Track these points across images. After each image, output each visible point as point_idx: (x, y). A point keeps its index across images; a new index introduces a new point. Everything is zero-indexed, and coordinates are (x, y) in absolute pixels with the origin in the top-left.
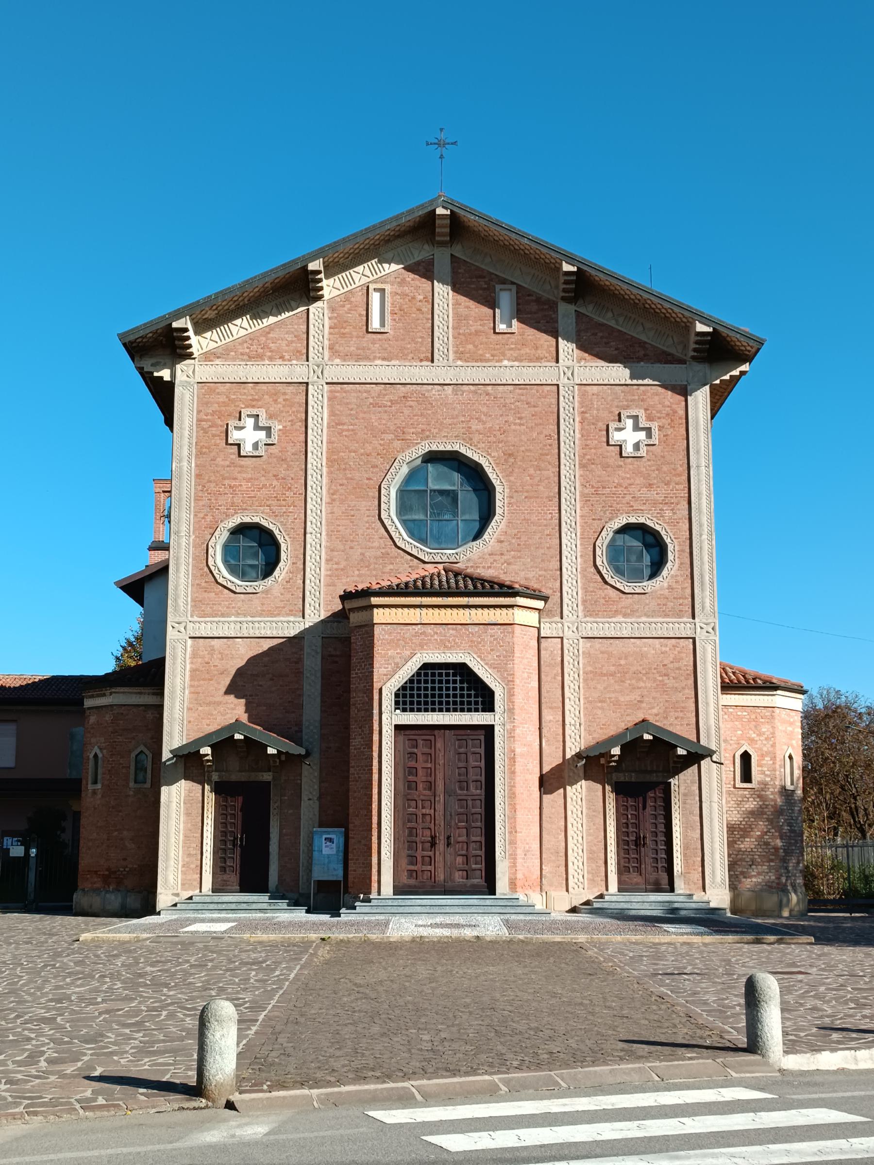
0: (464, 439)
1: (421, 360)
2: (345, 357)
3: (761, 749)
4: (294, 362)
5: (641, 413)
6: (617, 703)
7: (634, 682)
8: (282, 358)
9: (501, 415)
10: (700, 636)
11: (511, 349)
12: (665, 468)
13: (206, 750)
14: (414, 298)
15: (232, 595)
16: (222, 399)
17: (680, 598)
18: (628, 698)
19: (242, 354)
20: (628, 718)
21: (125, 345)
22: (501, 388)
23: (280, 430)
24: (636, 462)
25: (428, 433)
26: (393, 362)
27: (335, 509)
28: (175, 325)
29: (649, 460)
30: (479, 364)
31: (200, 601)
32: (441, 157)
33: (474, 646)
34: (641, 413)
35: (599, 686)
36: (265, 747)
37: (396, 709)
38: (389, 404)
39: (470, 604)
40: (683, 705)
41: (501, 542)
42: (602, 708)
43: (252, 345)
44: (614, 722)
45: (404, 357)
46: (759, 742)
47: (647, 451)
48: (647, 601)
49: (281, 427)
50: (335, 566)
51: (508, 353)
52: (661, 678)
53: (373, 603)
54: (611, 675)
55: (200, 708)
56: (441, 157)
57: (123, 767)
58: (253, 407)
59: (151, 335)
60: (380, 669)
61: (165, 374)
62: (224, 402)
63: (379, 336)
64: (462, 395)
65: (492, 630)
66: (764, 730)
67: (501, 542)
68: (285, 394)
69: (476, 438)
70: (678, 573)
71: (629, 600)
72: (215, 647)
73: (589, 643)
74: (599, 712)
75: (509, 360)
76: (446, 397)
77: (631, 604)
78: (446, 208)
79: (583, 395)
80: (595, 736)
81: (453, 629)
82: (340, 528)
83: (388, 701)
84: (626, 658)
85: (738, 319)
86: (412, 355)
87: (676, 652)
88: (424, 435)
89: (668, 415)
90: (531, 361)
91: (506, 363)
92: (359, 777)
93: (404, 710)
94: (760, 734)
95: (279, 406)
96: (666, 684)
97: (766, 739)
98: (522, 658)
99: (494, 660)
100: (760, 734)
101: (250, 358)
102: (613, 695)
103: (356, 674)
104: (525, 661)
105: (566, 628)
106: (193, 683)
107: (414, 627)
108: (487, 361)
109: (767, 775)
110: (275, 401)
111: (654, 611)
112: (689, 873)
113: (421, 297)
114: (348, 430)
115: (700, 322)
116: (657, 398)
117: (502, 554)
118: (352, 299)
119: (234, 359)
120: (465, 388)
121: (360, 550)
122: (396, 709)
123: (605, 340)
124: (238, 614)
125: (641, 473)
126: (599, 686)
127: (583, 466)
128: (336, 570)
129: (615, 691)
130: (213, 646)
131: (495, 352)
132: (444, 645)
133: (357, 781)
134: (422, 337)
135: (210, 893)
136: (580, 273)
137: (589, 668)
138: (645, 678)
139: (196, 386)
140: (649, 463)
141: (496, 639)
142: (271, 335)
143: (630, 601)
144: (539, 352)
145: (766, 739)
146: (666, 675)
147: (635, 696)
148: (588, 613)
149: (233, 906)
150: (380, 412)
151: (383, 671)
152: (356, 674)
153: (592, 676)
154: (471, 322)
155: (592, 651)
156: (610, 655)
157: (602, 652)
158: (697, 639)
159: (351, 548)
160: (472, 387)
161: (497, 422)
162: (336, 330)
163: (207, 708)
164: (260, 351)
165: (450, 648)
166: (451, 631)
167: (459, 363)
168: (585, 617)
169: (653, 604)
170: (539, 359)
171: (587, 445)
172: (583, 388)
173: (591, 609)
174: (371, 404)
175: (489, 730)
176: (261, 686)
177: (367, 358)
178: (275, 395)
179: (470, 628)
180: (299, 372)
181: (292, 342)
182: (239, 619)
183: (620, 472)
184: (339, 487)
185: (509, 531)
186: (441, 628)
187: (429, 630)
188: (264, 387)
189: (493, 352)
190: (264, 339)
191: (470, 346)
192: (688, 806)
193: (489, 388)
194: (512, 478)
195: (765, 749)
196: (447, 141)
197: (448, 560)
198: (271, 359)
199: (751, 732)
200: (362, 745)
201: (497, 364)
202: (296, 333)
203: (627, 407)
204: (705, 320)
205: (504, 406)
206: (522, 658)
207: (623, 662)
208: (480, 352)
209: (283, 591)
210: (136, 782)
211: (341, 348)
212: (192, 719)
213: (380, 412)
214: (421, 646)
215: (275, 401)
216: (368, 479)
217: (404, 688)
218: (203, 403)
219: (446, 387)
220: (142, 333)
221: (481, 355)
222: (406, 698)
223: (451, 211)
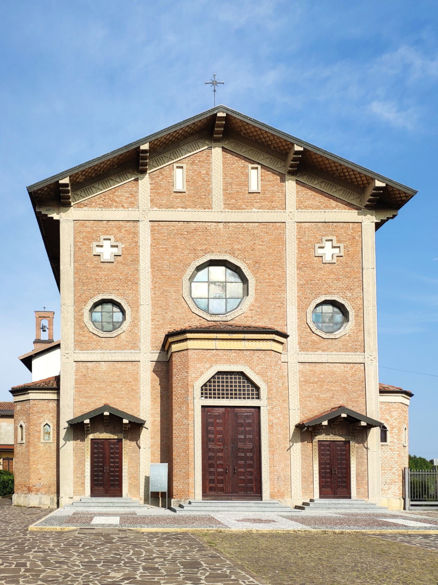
0: (230, 254)
1: (204, 209)
2: (160, 206)
3: (392, 425)
4: (131, 209)
5: (334, 238)
6: (318, 398)
7: (328, 387)
8: (123, 206)
9: (251, 240)
10: (367, 361)
11: (257, 202)
12: (348, 270)
13: (125, 421)
14: (200, 172)
15: (98, 338)
16: (89, 230)
17: (355, 342)
18: (325, 396)
19: (99, 204)
20: (325, 406)
21: (30, 194)
22: (251, 224)
23: (123, 248)
24: (332, 266)
25: (209, 250)
26: (188, 209)
27: (156, 292)
28: (61, 182)
29: (338, 265)
30: (239, 211)
31: (80, 342)
32: (215, 91)
33: (248, 363)
34: (334, 238)
35: (308, 389)
36: (122, 419)
37: (201, 397)
38: (186, 233)
39: (246, 338)
40: (357, 400)
41: (252, 310)
42: (309, 401)
43: (105, 199)
44: (318, 407)
45: (195, 206)
46: (391, 421)
47: (337, 260)
48: (336, 343)
49: (123, 246)
50: (157, 323)
51: (256, 205)
52: (344, 385)
53: (188, 337)
54: (315, 383)
55: (81, 400)
56: (215, 91)
57: (37, 432)
58: (107, 234)
59: (46, 189)
60: (192, 374)
61: (55, 216)
62: (89, 232)
63: (180, 194)
64: (229, 228)
65: (257, 354)
66: (394, 415)
67: (252, 310)
68: (126, 227)
69: (237, 253)
70: (354, 328)
71: (326, 342)
72: (89, 367)
73: (302, 366)
74: (308, 403)
75: (256, 208)
76: (220, 230)
77: (327, 345)
78: (224, 112)
79: (299, 228)
80: (306, 416)
81: (235, 353)
82: (159, 302)
83: (198, 392)
84: (324, 374)
85: (401, 178)
86: (198, 205)
87: (353, 371)
88: (206, 252)
89: (350, 239)
90: (269, 209)
91: (254, 210)
92: (180, 435)
93: (206, 397)
94: (392, 417)
95: (122, 234)
96: (347, 388)
97: (395, 419)
98: (275, 370)
99: (259, 370)
100: (392, 417)
101: (105, 207)
102: (317, 394)
103: (176, 378)
104: (276, 371)
105: (289, 357)
106: (77, 386)
107: (212, 351)
108: (244, 209)
109: (394, 438)
110: (120, 231)
111: (340, 349)
112: (359, 489)
113: (204, 172)
114: (162, 248)
115: (378, 180)
116: (343, 230)
117: (252, 317)
118: (164, 173)
119: (95, 207)
120: (230, 224)
121: (171, 314)
122: (201, 397)
123: (313, 197)
124: (101, 349)
125: (334, 272)
126: (308, 389)
127: (299, 268)
128: (158, 325)
129: (318, 392)
130: (88, 366)
131: (248, 204)
132: (228, 361)
133: (178, 437)
134: (205, 195)
135: (90, 497)
136: (305, 152)
137: (302, 379)
138: (335, 385)
139: (72, 222)
140: (338, 267)
141: (261, 358)
142: (116, 193)
143: (326, 343)
144: (274, 204)
145: (395, 419)
146: (347, 383)
147: (329, 394)
148: (302, 349)
149: (105, 504)
150: (181, 238)
151: (193, 375)
152: (176, 378)
153: (305, 382)
154: (234, 187)
155: (304, 370)
156: (315, 372)
157: (311, 371)
158: (366, 364)
159: (166, 313)
160: (234, 224)
161: (249, 243)
162: (154, 191)
163: (85, 400)
164: (110, 202)
165: (232, 363)
166: (234, 354)
167: (227, 210)
168: (300, 351)
169: (340, 345)
170: (274, 208)
171: (301, 257)
172: (300, 224)
173: (304, 347)
174: (176, 233)
175: (259, 408)
176: (116, 387)
177: (172, 207)
178: (119, 229)
179: (245, 352)
180: (132, 214)
181: (129, 198)
182: (102, 352)
183: (321, 272)
184: (158, 280)
185: (256, 305)
186: (227, 352)
187: (220, 353)
188: (113, 223)
189: (246, 204)
190: (112, 195)
191: (234, 201)
192: (359, 454)
193: (244, 224)
194: (258, 275)
195: (394, 424)
196: (218, 81)
197: (221, 320)
198: (116, 207)
199: (386, 416)
200: (181, 417)
201: (249, 211)
202: (130, 192)
203: (326, 235)
204: (382, 179)
205: (253, 235)
206: (275, 370)
207: (322, 376)
208: (239, 204)
209: (127, 336)
210: (44, 439)
211: (158, 201)
212: (77, 406)
213: (181, 238)
214: (216, 362)
215: (120, 231)
216: (174, 275)
217: (205, 385)
218: (77, 232)
219: (219, 224)
220: (41, 186)
221: (240, 206)
222: (207, 390)
223: (227, 114)
